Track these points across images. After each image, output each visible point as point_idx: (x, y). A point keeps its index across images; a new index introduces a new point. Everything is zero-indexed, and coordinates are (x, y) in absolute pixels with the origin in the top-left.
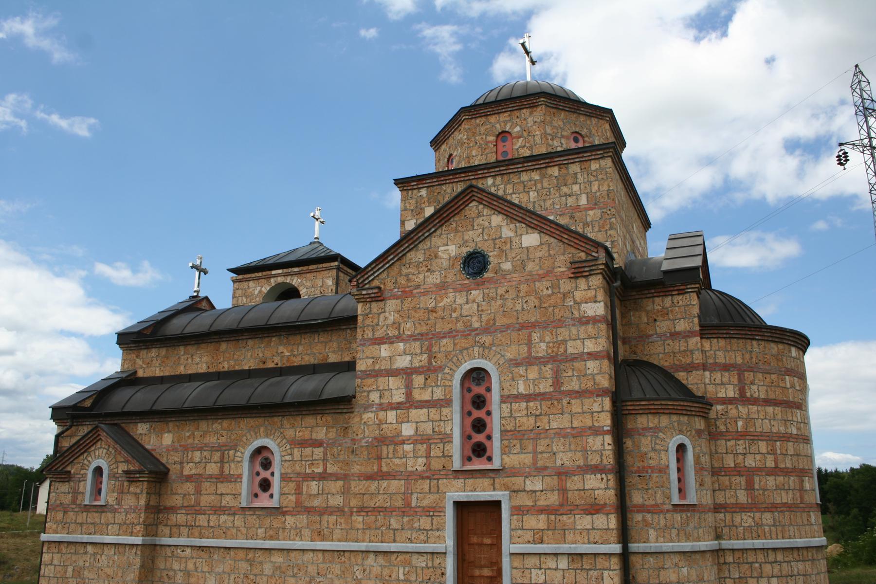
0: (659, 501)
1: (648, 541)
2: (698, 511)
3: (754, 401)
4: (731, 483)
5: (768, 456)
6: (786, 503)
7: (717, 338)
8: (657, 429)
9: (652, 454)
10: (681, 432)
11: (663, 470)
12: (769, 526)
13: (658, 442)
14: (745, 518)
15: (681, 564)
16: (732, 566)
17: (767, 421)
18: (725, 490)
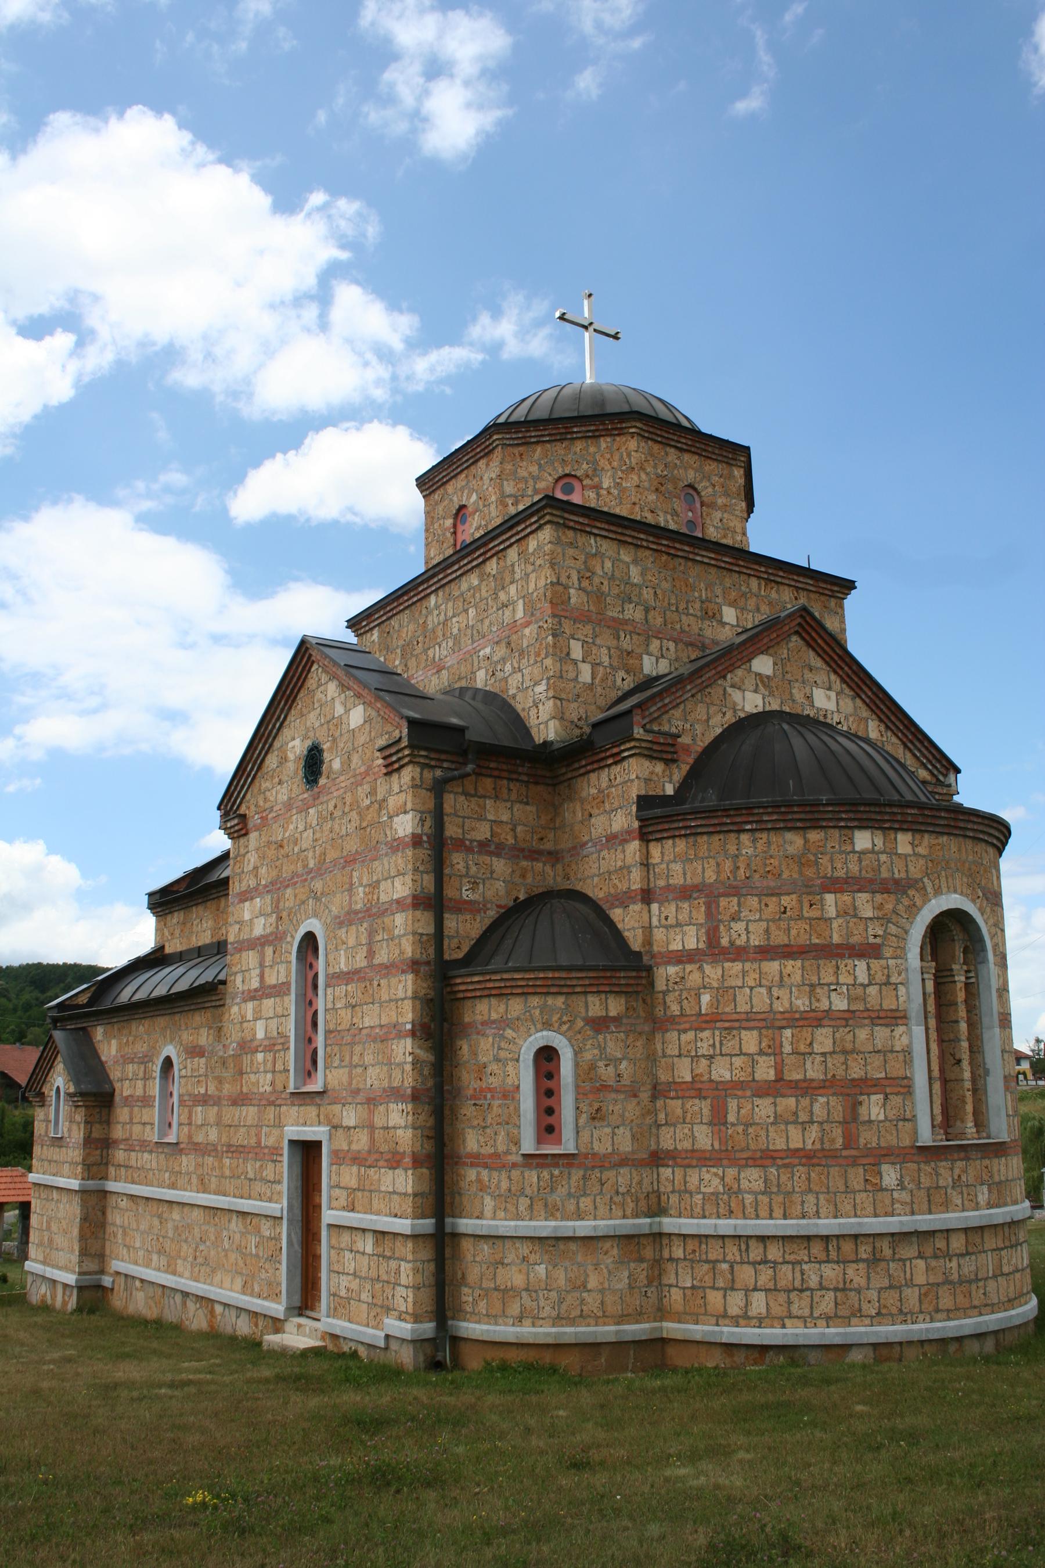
0: (501, 1148)
1: (482, 1218)
2: (580, 1166)
3: (738, 953)
4: (685, 1112)
5: (761, 1059)
6: (797, 1150)
7: (673, 837)
8: (504, 1023)
9: (493, 1067)
10: (547, 1025)
11: (511, 1094)
12: (755, 1193)
13: (503, 1045)
14: (707, 1177)
15: (532, 1258)
16: (681, 1265)
17: (763, 990)
18: (675, 1126)
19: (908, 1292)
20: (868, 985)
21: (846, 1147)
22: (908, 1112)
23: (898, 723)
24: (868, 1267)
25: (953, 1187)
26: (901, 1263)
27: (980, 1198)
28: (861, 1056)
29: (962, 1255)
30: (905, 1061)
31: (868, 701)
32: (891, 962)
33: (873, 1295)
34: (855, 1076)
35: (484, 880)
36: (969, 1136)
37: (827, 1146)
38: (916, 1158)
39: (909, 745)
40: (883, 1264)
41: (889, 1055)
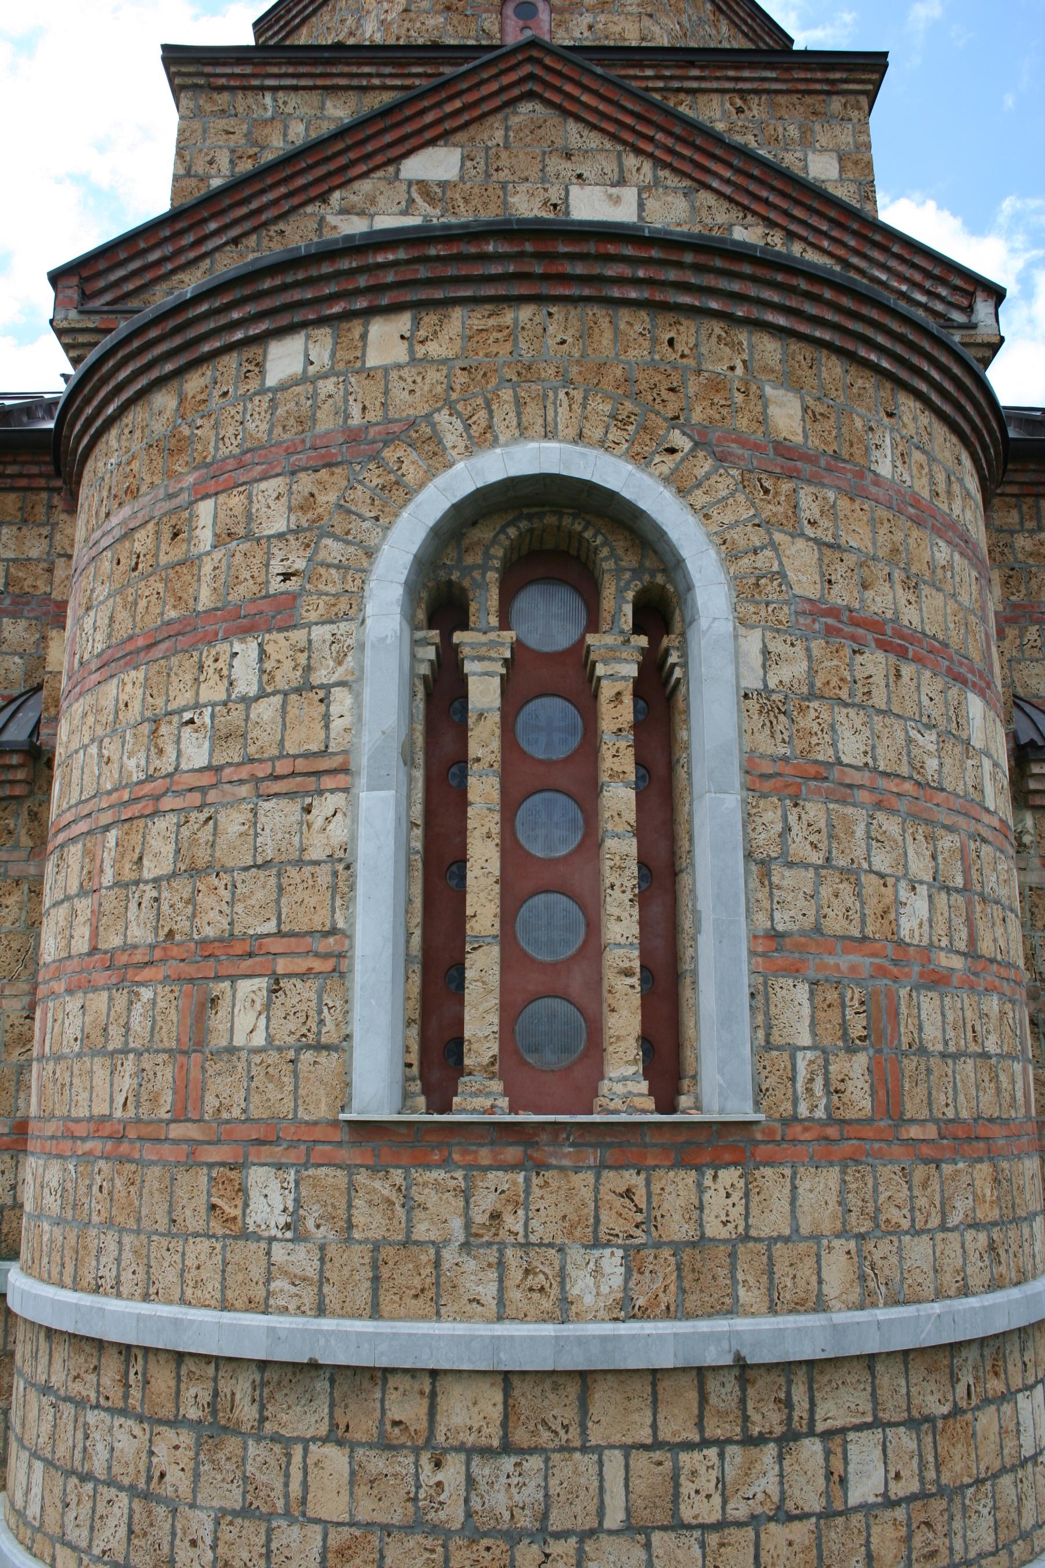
19: (289, 1535)
20: (257, 699)
21: (179, 1117)
22: (329, 1025)
23: (814, 221)
24: (199, 1445)
25: (465, 1246)
26: (277, 1448)
27: (581, 1285)
28: (226, 878)
29: (486, 1452)
30: (334, 888)
31: (728, 190)
32: (320, 633)
33: (201, 1523)
34: (209, 932)
36: (617, 1104)
37: (144, 1112)
38: (345, 1155)
39: (855, 260)
40: (232, 1444)
41: (292, 871)
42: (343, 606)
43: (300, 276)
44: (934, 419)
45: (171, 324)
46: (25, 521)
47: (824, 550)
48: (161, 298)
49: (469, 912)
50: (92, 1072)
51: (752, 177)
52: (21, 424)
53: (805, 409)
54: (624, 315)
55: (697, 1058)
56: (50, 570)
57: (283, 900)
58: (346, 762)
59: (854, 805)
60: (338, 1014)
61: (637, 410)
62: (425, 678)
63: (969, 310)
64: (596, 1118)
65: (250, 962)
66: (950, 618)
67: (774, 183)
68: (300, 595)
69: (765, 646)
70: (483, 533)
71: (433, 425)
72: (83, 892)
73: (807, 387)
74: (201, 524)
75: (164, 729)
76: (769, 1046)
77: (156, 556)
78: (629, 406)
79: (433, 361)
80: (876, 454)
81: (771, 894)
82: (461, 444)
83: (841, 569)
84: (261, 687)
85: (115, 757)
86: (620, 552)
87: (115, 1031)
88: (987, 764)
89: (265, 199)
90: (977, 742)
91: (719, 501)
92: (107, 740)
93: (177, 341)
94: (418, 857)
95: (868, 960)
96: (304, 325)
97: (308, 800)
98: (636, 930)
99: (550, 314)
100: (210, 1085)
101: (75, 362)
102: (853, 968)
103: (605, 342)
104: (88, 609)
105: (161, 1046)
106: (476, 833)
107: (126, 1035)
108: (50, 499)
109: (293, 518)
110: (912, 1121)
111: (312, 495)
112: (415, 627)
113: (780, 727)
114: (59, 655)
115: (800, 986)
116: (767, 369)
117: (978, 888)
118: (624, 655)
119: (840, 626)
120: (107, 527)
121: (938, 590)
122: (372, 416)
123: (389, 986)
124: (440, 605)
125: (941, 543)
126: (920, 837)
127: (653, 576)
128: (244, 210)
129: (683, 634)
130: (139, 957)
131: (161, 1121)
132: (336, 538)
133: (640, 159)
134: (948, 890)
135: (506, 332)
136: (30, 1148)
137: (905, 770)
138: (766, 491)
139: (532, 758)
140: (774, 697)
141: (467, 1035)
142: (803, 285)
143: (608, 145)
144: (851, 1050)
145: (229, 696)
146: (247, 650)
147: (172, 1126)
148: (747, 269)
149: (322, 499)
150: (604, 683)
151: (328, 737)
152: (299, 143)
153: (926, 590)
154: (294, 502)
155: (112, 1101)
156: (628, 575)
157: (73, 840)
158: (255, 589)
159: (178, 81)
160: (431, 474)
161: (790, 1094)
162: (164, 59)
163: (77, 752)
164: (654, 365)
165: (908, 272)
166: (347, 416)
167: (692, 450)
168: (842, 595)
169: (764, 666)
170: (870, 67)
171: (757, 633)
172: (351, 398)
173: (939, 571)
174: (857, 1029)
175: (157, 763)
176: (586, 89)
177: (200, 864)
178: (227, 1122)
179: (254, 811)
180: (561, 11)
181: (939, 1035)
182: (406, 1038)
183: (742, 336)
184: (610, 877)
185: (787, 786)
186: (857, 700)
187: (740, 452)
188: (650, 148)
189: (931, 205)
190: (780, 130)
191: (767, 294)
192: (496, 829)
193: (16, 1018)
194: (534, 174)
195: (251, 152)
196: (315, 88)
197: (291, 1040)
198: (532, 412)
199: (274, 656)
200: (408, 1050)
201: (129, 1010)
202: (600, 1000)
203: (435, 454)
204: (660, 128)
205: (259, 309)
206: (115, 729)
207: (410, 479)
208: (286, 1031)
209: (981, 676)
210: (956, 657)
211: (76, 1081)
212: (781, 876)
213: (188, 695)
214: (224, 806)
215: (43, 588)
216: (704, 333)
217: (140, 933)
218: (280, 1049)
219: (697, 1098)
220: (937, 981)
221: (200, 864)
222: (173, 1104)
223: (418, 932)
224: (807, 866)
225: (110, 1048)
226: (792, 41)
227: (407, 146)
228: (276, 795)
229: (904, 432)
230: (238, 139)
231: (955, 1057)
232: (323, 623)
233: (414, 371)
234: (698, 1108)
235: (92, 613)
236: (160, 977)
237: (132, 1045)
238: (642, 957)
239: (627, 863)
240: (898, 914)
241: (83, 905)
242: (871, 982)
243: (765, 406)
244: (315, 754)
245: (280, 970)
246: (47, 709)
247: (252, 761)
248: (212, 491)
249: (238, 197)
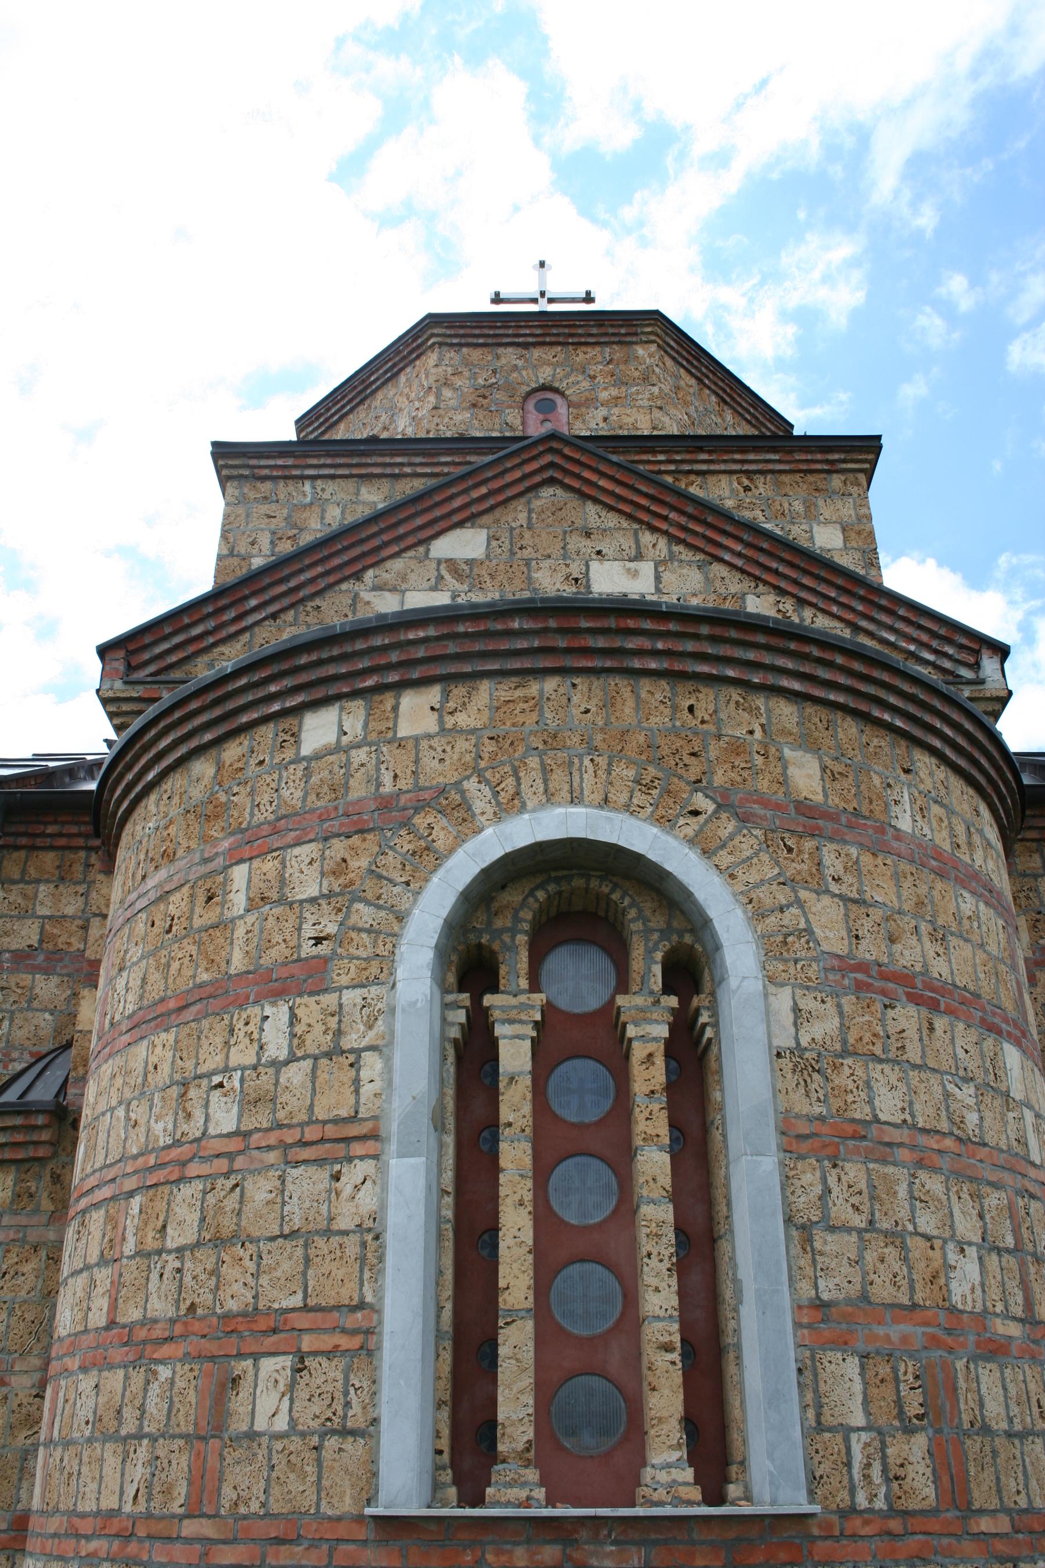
20: (287, 1063)
22: (356, 1408)
23: (822, 588)
28: (251, 1248)
30: (362, 1260)
31: (739, 563)
32: (351, 997)
34: (232, 1305)
35: (12, 1013)
36: (661, 1494)
39: (864, 624)
41: (320, 1242)
42: (374, 970)
43: (336, 652)
44: (950, 773)
45: (212, 696)
46: (62, 879)
47: (850, 905)
48: (203, 671)
49: (502, 1283)
50: (102, 1460)
51: (761, 550)
52: (63, 785)
53: (824, 769)
54: (645, 685)
55: (745, 1442)
56: (85, 928)
57: (310, 1272)
58: (376, 1128)
59: (895, 1164)
60: (365, 1396)
61: (660, 775)
62: (455, 1041)
63: (976, 666)
64: (639, 1511)
65: (274, 1338)
66: (979, 969)
67: (783, 555)
68: (331, 959)
69: (795, 1004)
70: (512, 897)
71: (463, 793)
72: (103, 1261)
73: (824, 748)
74: (235, 888)
75: (192, 1093)
76: (820, 1427)
77: (190, 919)
78: (652, 771)
79: (462, 731)
80: (895, 810)
81: (814, 1261)
82: (490, 811)
83: (868, 923)
84: (291, 1051)
85: (142, 1121)
86: (648, 913)
87: (128, 1413)
88: (1029, 1116)
89: (302, 578)
90: (1017, 1094)
91: (743, 861)
92: (135, 1103)
93: (217, 712)
94: (449, 1226)
95: (920, 1330)
96: (339, 697)
97: (337, 1167)
98: (675, 1301)
99: (574, 685)
100: (228, 1476)
101: (118, 729)
102: (905, 1339)
103: (627, 711)
104: (121, 970)
105: (177, 1430)
106: (509, 1201)
107: (141, 1419)
108: (88, 857)
109: (325, 883)
110: (981, 1511)
111: (344, 860)
112: (445, 991)
113: (815, 1086)
114: (90, 1014)
115: (849, 1359)
116: (784, 732)
117: (1030, 1247)
118: (655, 1016)
119: (873, 982)
120: (143, 889)
121: (966, 940)
122: (403, 784)
123: (419, 1365)
124: (469, 966)
125: (966, 894)
126: (965, 1196)
127: (681, 935)
128: (283, 588)
129: (713, 994)
130: (158, 1332)
131: (173, 1516)
132: (368, 903)
133: (656, 536)
134: (999, 1251)
135: (532, 703)
136: (29, 1547)
137: (944, 1126)
138: (790, 850)
139: (565, 1122)
140: (807, 1055)
141: (501, 1417)
142: (816, 652)
143: (625, 524)
144: (909, 1431)
145: (259, 1060)
146: (278, 1014)
147: (186, 1522)
148: (761, 639)
149: (353, 864)
150: (635, 1044)
151: (357, 1102)
152: (335, 526)
153: (953, 941)
154: (326, 867)
155: (122, 1493)
156: (656, 936)
157: (96, 1206)
158: (287, 952)
159: (224, 472)
160: (460, 840)
161: (845, 1482)
162: (213, 454)
163: (103, 1114)
164: (675, 731)
165: (915, 633)
166: (379, 785)
167: (715, 812)
168: (870, 950)
169: (795, 1024)
170: (867, 448)
171: (787, 991)
172: (383, 767)
173: (965, 922)
174: (913, 1408)
175: (185, 1127)
176: (602, 475)
177: (226, 1233)
178: (245, 1517)
179: (282, 1179)
180: (578, 406)
181: (1002, 1411)
182: (436, 1421)
183: (760, 701)
184: (646, 1245)
185: (825, 1146)
186: (891, 1055)
187: (762, 812)
188: (664, 526)
189: (931, 563)
190: (786, 505)
191: (781, 662)
192: (528, 1197)
193: (24, 1397)
194: (556, 551)
195: (290, 534)
196: (351, 476)
197: (315, 1424)
198: (559, 778)
199: (305, 1020)
200: (438, 1435)
201: (146, 1390)
202: (639, 1377)
203: (464, 820)
204: (673, 508)
205: (296, 683)
206: (143, 1091)
207: (440, 845)
208: (311, 1413)
209: (1016, 1025)
210: (988, 1008)
211: (85, 1469)
212: (826, 1242)
213: (218, 1058)
214: (252, 1172)
215: (77, 945)
216: (722, 699)
217: (160, 1306)
218: (303, 1435)
219: (747, 1488)
220: (994, 1350)
221: (226, 1233)
222: (188, 1496)
223: (449, 1306)
224: (849, 1230)
225: (123, 1432)
226: (792, 426)
227: (437, 528)
228: (305, 1162)
229: (921, 787)
230: (278, 523)
231: (1022, 1436)
232: (354, 987)
233: (444, 740)
234: (748, 1498)
235: (125, 974)
236: (180, 1353)
237: (146, 1430)
238: (682, 1330)
239: (664, 1230)
240: (948, 1278)
241: (103, 1276)
242: (924, 1354)
243: (785, 768)
244: (344, 1120)
245: (305, 1348)
246: (75, 1068)
247: (280, 1126)
248: (247, 856)
249: (277, 576)
